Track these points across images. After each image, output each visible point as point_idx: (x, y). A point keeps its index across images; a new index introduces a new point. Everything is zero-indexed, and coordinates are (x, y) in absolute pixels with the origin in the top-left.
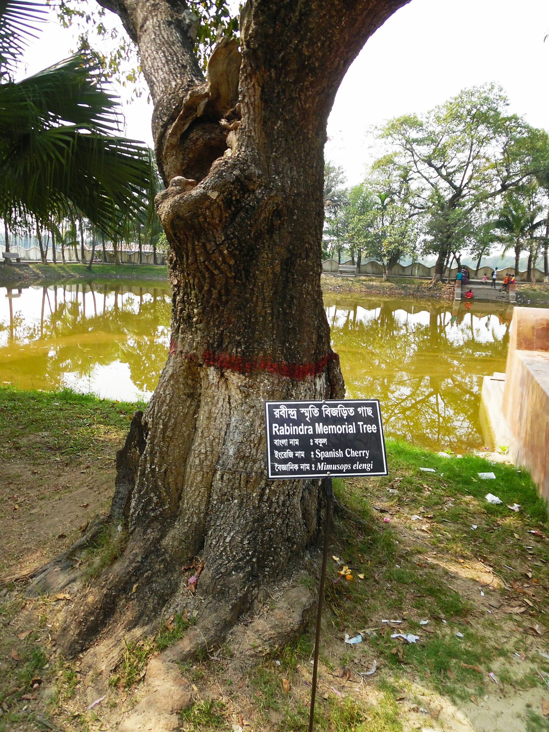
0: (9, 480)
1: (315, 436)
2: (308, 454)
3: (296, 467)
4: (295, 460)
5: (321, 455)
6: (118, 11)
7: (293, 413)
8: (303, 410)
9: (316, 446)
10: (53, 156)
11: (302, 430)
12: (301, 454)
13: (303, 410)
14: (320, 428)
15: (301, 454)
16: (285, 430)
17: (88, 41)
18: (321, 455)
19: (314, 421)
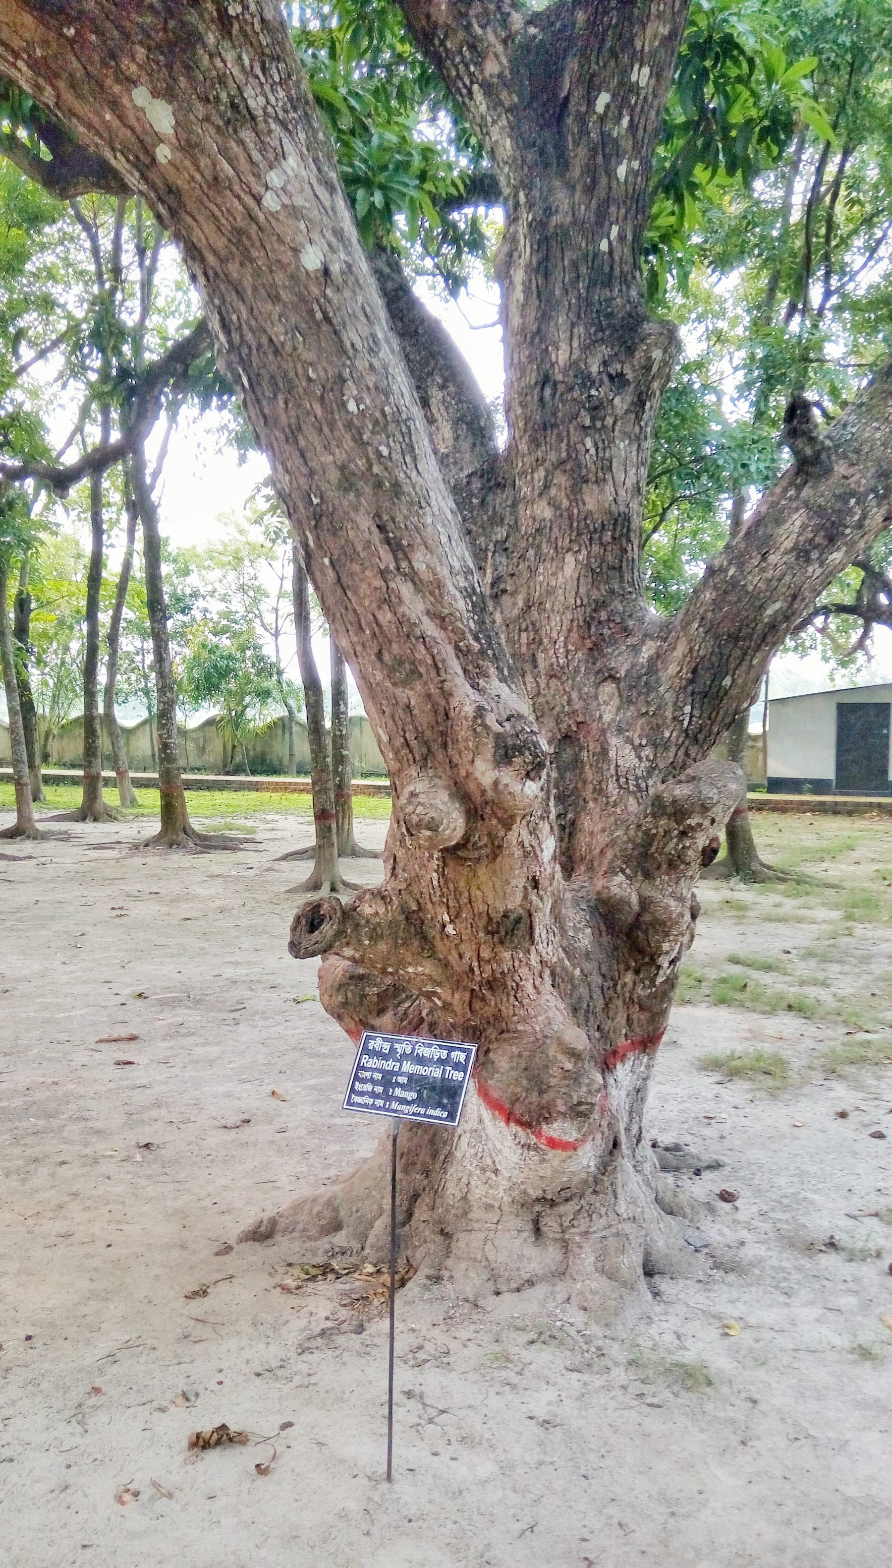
0: (891, 1217)
1: (399, 1073)
2: (385, 1091)
3: (371, 1101)
4: (374, 1095)
5: (398, 1092)
6: (182, 245)
7: (387, 1046)
8: (396, 1046)
9: (398, 1084)
10: (126, 233)
11: (389, 1065)
12: (379, 1089)
13: (396, 1046)
14: (407, 1067)
15: (379, 1089)
16: (373, 1063)
17: (159, 510)
18: (398, 1092)
19: (404, 1056)
